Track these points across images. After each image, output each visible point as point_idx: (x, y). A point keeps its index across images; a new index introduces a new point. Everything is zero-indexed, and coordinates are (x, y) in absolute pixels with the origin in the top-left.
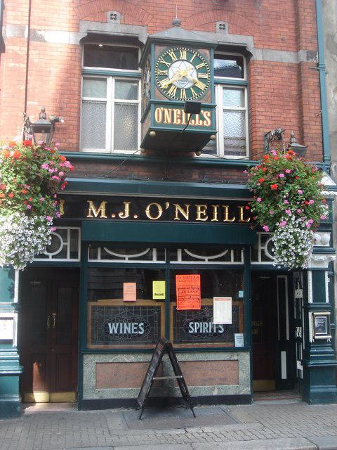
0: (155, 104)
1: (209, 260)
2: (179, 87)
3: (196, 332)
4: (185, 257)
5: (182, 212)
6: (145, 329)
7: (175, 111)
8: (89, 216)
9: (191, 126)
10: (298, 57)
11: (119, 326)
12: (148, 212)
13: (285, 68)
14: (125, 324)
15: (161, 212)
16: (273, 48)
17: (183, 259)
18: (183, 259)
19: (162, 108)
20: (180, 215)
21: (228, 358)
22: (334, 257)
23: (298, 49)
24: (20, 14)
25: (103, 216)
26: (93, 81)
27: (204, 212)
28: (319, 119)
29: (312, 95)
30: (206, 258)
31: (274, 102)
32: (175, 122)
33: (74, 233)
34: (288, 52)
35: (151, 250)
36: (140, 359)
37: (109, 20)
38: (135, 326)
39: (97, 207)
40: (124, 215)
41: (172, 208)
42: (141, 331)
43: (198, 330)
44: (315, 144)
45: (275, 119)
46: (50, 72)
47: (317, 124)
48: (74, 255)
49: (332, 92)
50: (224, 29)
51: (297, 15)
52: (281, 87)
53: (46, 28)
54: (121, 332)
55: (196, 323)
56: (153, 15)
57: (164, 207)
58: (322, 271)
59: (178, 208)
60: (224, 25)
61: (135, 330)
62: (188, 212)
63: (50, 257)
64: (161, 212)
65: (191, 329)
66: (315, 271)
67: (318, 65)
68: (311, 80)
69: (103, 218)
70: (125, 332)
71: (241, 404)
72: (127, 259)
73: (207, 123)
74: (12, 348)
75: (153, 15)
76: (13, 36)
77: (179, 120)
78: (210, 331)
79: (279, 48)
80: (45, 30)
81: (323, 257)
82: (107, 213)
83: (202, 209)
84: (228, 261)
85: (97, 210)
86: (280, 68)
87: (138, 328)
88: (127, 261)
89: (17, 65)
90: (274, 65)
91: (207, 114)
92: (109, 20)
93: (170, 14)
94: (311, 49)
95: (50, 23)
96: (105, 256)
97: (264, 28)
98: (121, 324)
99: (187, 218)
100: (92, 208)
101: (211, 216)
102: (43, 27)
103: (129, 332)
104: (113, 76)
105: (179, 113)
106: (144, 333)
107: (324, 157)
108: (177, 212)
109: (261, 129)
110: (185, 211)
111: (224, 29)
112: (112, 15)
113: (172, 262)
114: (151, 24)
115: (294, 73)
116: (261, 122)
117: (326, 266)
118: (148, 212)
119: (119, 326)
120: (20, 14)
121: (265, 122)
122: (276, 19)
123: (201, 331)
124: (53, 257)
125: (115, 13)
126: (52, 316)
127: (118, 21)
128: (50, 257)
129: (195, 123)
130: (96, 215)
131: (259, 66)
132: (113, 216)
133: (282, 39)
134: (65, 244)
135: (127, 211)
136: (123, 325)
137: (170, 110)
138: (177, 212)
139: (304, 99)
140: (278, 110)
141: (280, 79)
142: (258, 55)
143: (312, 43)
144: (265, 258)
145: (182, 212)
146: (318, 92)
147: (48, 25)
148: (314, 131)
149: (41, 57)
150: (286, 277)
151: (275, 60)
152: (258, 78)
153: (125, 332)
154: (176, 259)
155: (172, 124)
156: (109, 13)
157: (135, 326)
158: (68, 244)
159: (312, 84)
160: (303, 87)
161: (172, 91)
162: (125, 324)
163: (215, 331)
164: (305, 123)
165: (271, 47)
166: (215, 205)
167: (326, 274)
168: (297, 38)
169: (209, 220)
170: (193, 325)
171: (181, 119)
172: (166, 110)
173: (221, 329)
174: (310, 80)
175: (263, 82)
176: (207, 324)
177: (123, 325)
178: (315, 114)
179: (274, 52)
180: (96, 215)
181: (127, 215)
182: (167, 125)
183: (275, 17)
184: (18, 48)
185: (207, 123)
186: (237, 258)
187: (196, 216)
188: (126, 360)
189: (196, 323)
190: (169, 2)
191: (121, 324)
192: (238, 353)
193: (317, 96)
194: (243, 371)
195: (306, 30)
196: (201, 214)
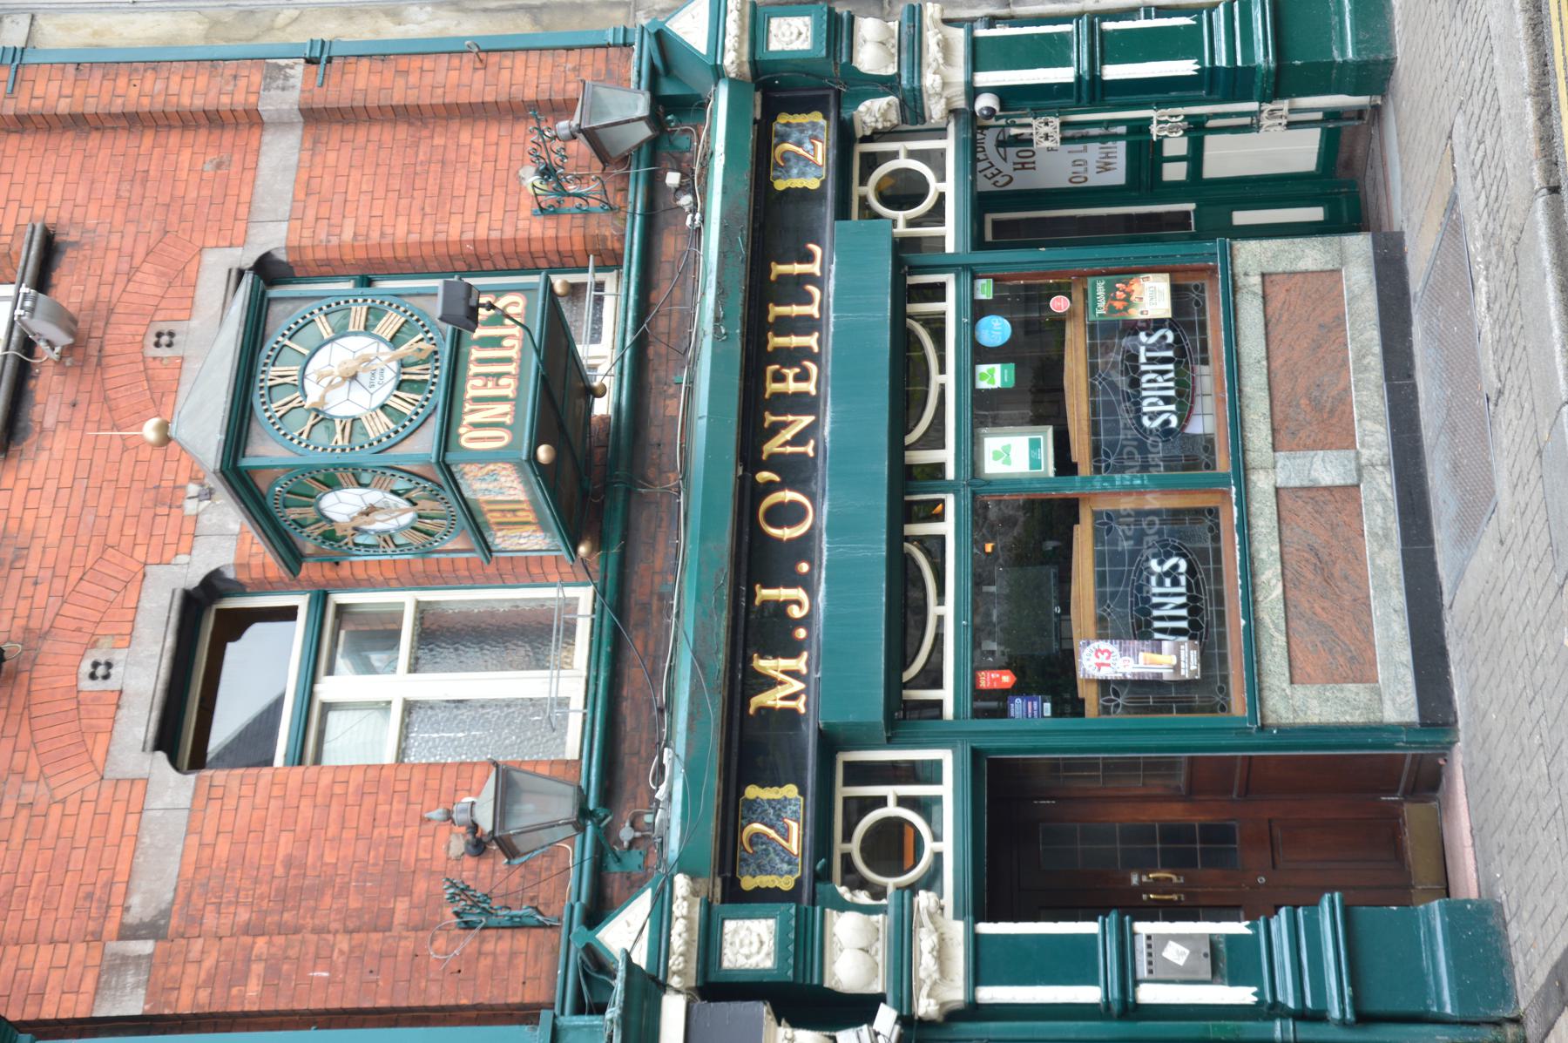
0: (446, 450)
1: (942, 370)
2: (393, 384)
3: (1172, 407)
4: (934, 438)
5: (787, 435)
6: (1169, 556)
7: (471, 393)
8: (800, 705)
9: (518, 389)
10: (282, 124)
11: (1163, 631)
12: (786, 533)
13: (318, 159)
14: (1156, 613)
15: (788, 495)
16: (245, 191)
17: (941, 445)
18: (941, 445)
19: (462, 430)
20: (799, 439)
21: (1258, 302)
22: (932, 11)
23: (252, 120)
24: (56, 976)
25: (800, 664)
26: (326, 747)
27: (790, 373)
28: (494, 58)
29: (413, 79)
30: (936, 379)
31: (432, 187)
32: (510, 393)
33: (862, 773)
34: (264, 148)
35: (909, 539)
36: (1272, 553)
37: (113, 684)
38: (1161, 583)
39: (770, 683)
40: (799, 603)
41: (775, 463)
42: (1175, 567)
43: (1167, 400)
44: (574, 69)
45: (487, 190)
46: (289, 863)
47: (507, 63)
48: (929, 772)
49: (402, 28)
50: (171, 334)
51: (134, 121)
52: (383, 170)
53: (119, 889)
54: (1184, 624)
55: (1145, 409)
56: (106, 547)
57: (771, 487)
58: (974, 44)
59: (773, 447)
60: (159, 335)
61: (1175, 583)
62: (790, 418)
63: (937, 846)
64: (788, 495)
65: (1167, 422)
66: (977, 976)
67: (309, 61)
68: (362, 84)
69: (808, 664)
70: (1184, 612)
71: (1452, 691)
72: (940, 610)
73: (516, 304)
74: (1254, 939)
75: (106, 547)
76: (142, 992)
77: (503, 381)
78: (1171, 367)
79: (248, 176)
80: (127, 894)
81: (931, 38)
82: (793, 650)
83: (780, 378)
84: (943, 321)
85: (781, 683)
86: (317, 172)
87: (1167, 574)
88: (948, 610)
89: (258, 968)
90: (306, 188)
91: (474, 387)
92: (113, 684)
93: (108, 493)
94: (256, 78)
95: (104, 876)
96: (932, 677)
97: (174, 218)
98: (1157, 624)
99: (807, 420)
100: (771, 699)
101: (805, 353)
102: (116, 900)
103: (1183, 600)
104: (314, 680)
105: (479, 382)
106: (1183, 556)
107: (615, 45)
108: (789, 449)
109: (521, 224)
110: (785, 425)
111: (171, 334)
112: (93, 676)
113: (950, 474)
114: (140, 553)
115: (335, 133)
116: (497, 225)
117: (958, 35)
118: (786, 533)
119: (1163, 631)
120: (56, 976)
121: (498, 214)
122: (145, 181)
123: (1172, 393)
124: (942, 179)
125: (86, 667)
126: (1144, 888)
127: (119, 656)
128: (937, 846)
129: (512, 336)
130: (797, 686)
131: (307, 233)
132: (801, 633)
133: (219, 166)
134: (902, 154)
135: (782, 593)
136: (1161, 618)
137: (468, 407)
138: (789, 449)
139: (426, 100)
140: (460, 179)
141: (356, 175)
142: (271, 237)
143: (235, 77)
144: (937, 214)
145: (787, 435)
146: (403, 63)
147: (110, 884)
148: (532, 72)
149: (229, 896)
150: (989, 218)
151: (289, 187)
152: (347, 235)
153: (1184, 612)
154: (940, 468)
155: (517, 401)
156: (86, 685)
157: (1161, 583)
158: (891, 791)
159: (376, 80)
160: (383, 103)
161: (405, 404)
162: (1156, 613)
163: (1170, 354)
164: (503, 98)
165: (245, 197)
166: (767, 342)
167: (981, 32)
168: (214, 120)
169: (815, 358)
170: (1153, 417)
171: (499, 375)
172: (468, 419)
173: (1164, 337)
174: (361, 84)
175: (364, 220)
176: (1145, 378)
177: (1161, 618)
178: (475, 69)
179: (259, 190)
180: (797, 686)
181: (799, 593)
182: (517, 414)
183: (138, 190)
184: (191, 969)
185: (516, 304)
186: (937, 292)
187: (800, 396)
188: (1279, 590)
189: (1145, 409)
190: (9, 602)
191: (1157, 624)
192: (1239, 269)
193: (416, 62)
194: (1298, 258)
195: (192, 93)
196: (797, 378)
